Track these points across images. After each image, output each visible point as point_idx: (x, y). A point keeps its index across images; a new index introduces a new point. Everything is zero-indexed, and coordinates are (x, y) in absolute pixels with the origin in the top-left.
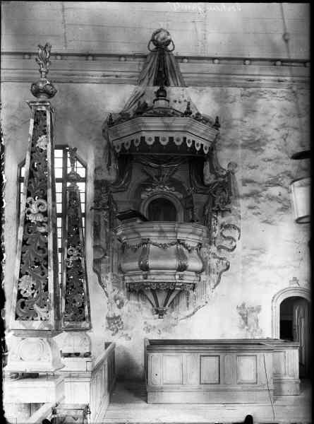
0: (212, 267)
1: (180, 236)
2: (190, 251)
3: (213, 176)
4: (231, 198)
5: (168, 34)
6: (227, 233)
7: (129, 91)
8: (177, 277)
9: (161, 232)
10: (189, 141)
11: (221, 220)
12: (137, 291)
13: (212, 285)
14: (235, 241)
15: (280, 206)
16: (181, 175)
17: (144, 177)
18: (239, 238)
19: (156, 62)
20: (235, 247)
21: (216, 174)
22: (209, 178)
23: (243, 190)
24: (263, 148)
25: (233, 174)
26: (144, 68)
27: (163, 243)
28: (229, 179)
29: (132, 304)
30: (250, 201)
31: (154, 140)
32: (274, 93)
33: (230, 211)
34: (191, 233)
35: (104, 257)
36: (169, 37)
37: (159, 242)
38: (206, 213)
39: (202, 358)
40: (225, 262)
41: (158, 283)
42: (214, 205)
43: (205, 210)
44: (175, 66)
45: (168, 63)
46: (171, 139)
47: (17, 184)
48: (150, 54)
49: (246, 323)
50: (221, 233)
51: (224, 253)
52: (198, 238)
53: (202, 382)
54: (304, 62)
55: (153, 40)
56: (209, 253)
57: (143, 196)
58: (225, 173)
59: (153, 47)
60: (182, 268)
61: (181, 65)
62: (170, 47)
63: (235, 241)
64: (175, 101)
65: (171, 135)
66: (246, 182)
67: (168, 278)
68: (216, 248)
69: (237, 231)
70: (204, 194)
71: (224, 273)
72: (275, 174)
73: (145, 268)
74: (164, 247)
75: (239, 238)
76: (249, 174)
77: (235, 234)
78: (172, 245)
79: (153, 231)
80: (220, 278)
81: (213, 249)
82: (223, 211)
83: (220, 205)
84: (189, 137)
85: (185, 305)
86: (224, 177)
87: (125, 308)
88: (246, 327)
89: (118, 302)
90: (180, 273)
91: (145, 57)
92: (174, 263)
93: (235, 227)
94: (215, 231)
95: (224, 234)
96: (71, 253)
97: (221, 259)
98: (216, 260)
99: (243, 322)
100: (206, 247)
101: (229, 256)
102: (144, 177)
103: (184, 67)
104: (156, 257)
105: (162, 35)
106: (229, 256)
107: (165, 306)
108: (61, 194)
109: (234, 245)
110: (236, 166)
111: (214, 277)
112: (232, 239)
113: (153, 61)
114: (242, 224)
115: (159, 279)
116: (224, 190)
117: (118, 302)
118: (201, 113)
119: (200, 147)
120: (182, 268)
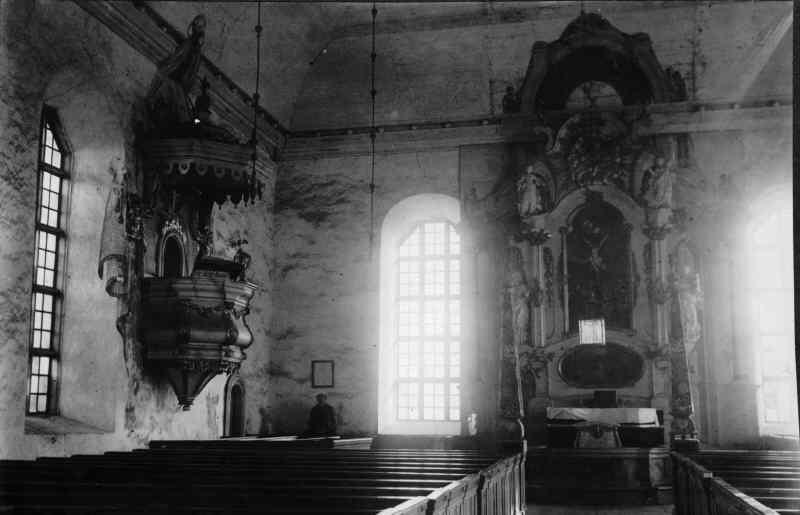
55: (193, 24)
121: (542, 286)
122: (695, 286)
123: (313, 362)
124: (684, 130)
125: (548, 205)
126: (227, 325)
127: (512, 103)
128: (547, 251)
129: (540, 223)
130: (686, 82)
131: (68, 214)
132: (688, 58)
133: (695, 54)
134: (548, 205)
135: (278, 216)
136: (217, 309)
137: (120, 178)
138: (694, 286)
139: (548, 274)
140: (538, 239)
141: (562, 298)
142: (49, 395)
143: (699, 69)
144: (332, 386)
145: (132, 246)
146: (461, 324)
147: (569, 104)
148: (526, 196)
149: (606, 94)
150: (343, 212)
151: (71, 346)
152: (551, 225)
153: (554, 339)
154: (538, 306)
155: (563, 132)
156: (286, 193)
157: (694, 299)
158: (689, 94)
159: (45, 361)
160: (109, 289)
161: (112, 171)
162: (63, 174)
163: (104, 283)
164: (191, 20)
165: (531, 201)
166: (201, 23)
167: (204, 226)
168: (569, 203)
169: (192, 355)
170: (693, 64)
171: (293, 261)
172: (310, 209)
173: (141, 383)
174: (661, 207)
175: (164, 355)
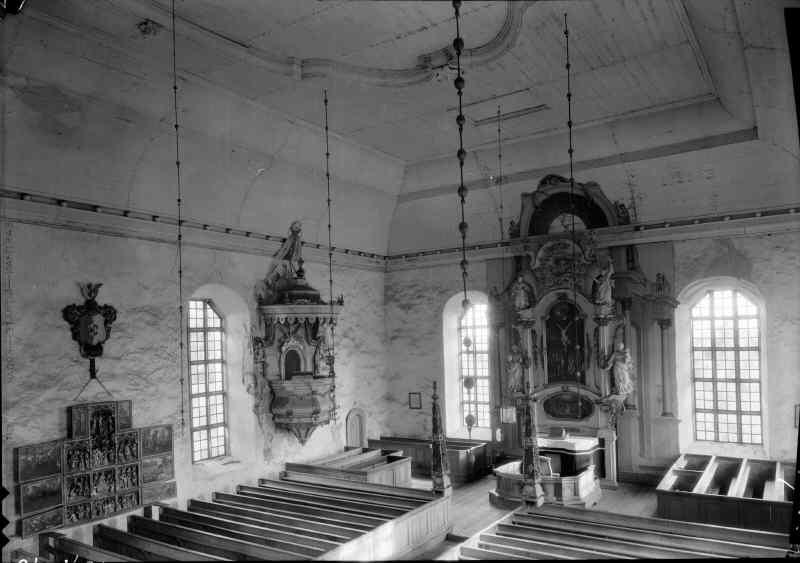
55: (291, 228)
121: (530, 355)
122: (626, 357)
123: (420, 394)
124: (630, 242)
125: (532, 302)
126: (314, 402)
127: (515, 233)
128: (533, 332)
129: (527, 315)
130: (630, 211)
131: (226, 351)
132: (629, 195)
133: (632, 191)
134: (532, 302)
135: (386, 307)
136: (308, 395)
137: (249, 330)
138: (624, 361)
139: (535, 346)
140: (528, 324)
141: (543, 360)
142: (225, 445)
143: (637, 201)
144: (420, 408)
145: (259, 365)
146: (489, 378)
147: (551, 231)
148: (518, 298)
149: (579, 224)
150: (421, 303)
151: (233, 423)
152: (536, 315)
153: (538, 389)
154: (527, 368)
155: (541, 254)
156: (390, 293)
157: (625, 367)
158: (632, 218)
159: (221, 429)
160: (248, 390)
161: (245, 326)
162: (222, 329)
163: (245, 388)
164: (289, 226)
165: (521, 300)
166: (297, 225)
167: (50, 547)
168: (548, 299)
169: (295, 421)
170: (632, 198)
171: (396, 334)
172: (404, 302)
173: (274, 435)
174: (603, 304)
175: (282, 420)
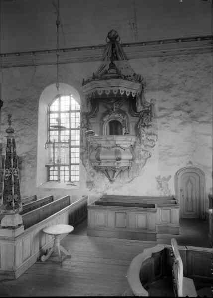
0: (142, 156)
1: (117, 143)
2: (124, 150)
3: (142, 107)
4: (152, 118)
5: (116, 32)
6: (150, 137)
7: (99, 64)
8: (116, 164)
9: (107, 140)
10: (122, 91)
11: (147, 130)
12: (98, 169)
13: (142, 165)
14: (155, 142)
15: (181, 121)
16: (125, 108)
17: (105, 110)
18: (157, 140)
19: (110, 48)
20: (155, 145)
21: (144, 106)
22: (140, 108)
23: (159, 114)
24: (170, 89)
25: (154, 105)
26: (104, 52)
27: (108, 146)
28: (152, 108)
29: (99, 175)
30: (164, 120)
31: (110, 92)
32: (178, 58)
33: (151, 125)
34: (124, 140)
35: (85, 152)
36: (117, 34)
37: (106, 146)
38: (138, 127)
39: (117, 214)
40: (149, 153)
41: (107, 167)
42: (142, 122)
43: (137, 126)
44: (121, 50)
45: (117, 48)
46: (111, 91)
47: (47, 115)
48: (108, 45)
49: (161, 187)
50: (147, 138)
51: (148, 148)
52: (129, 142)
53: (117, 226)
54: (210, 37)
55: (108, 37)
56: (140, 148)
57: (105, 119)
58: (149, 105)
59: (108, 40)
60: (119, 159)
61: (124, 48)
62: (118, 40)
63: (155, 142)
64: (122, 68)
65: (111, 89)
66: (161, 109)
67: (110, 165)
68: (144, 146)
69: (156, 136)
70: (136, 117)
71: (149, 159)
72: (178, 103)
73: (99, 159)
74: (108, 148)
75: (157, 140)
76: (162, 105)
77: (154, 137)
78: (113, 147)
79: (103, 140)
80: (146, 162)
81: (142, 146)
82: (148, 126)
83: (146, 122)
84: (121, 89)
85: (127, 176)
86: (148, 107)
87: (96, 177)
88: (161, 189)
89: (92, 174)
90: (118, 162)
91: (105, 46)
92: (113, 157)
93: (154, 134)
94: (143, 136)
95: (148, 138)
96: (7, 172)
97: (147, 151)
98: (144, 152)
99: (159, 186)
100: (138, 145)
101: (151, 151)
102: (105, 110)
103: (125, 49)
104: (105, 154)
105: (113, 33)
106: (151, 151)
107: (113, 177)
108: (79, 114)
109: (154, 144)
110: (155, 100)
111: (142, 161)
112: (153, 140)
113: (109, 48)
114: (159, 132)
115: (106, 165)
116: (148, 115)
117: (92, 174)
118: (137, 73)
119: (123, 93)
120: (119, 159)
